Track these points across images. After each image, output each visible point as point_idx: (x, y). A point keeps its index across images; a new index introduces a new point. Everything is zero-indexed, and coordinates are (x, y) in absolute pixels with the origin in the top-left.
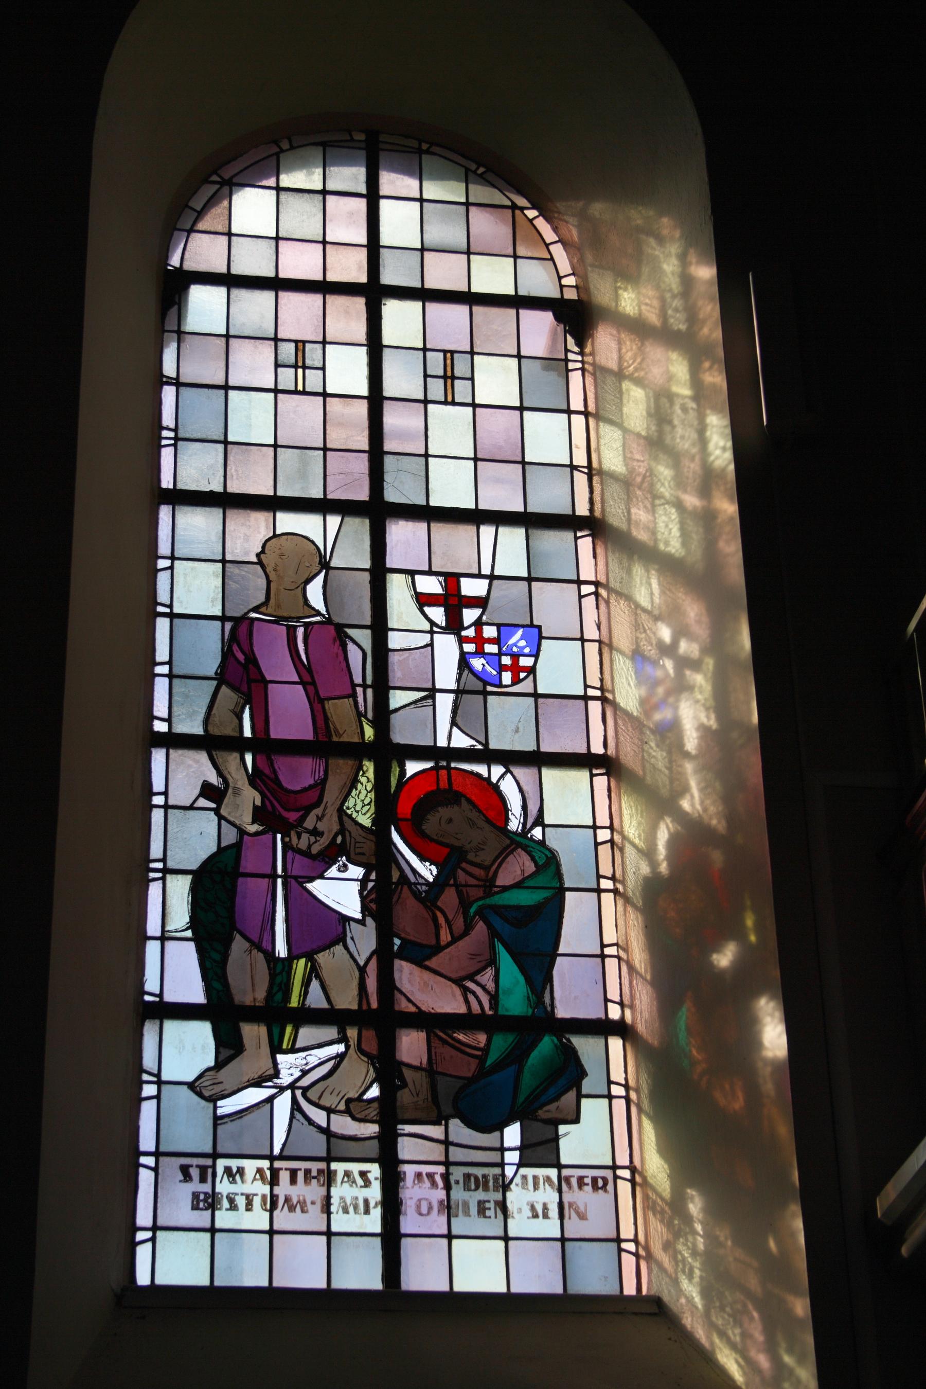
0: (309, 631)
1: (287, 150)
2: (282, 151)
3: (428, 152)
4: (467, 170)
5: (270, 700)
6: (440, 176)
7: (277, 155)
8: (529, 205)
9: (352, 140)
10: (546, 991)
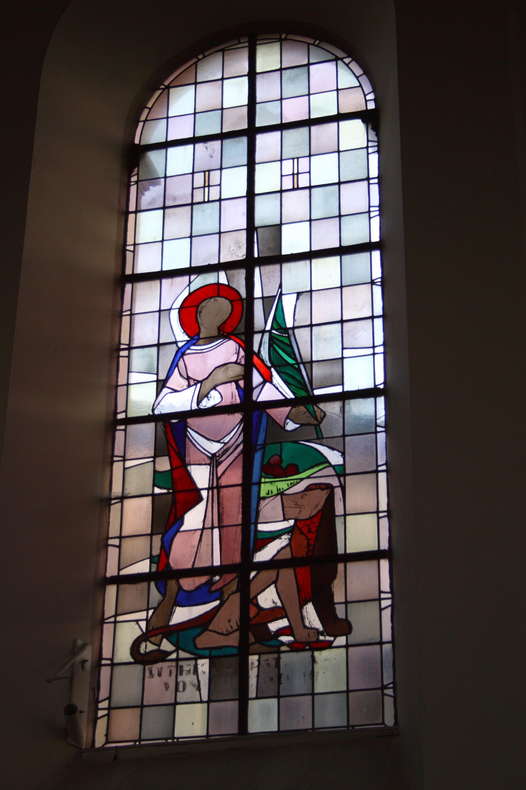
3: (286, 39)
4: (309, 44)
7: (196, 63)
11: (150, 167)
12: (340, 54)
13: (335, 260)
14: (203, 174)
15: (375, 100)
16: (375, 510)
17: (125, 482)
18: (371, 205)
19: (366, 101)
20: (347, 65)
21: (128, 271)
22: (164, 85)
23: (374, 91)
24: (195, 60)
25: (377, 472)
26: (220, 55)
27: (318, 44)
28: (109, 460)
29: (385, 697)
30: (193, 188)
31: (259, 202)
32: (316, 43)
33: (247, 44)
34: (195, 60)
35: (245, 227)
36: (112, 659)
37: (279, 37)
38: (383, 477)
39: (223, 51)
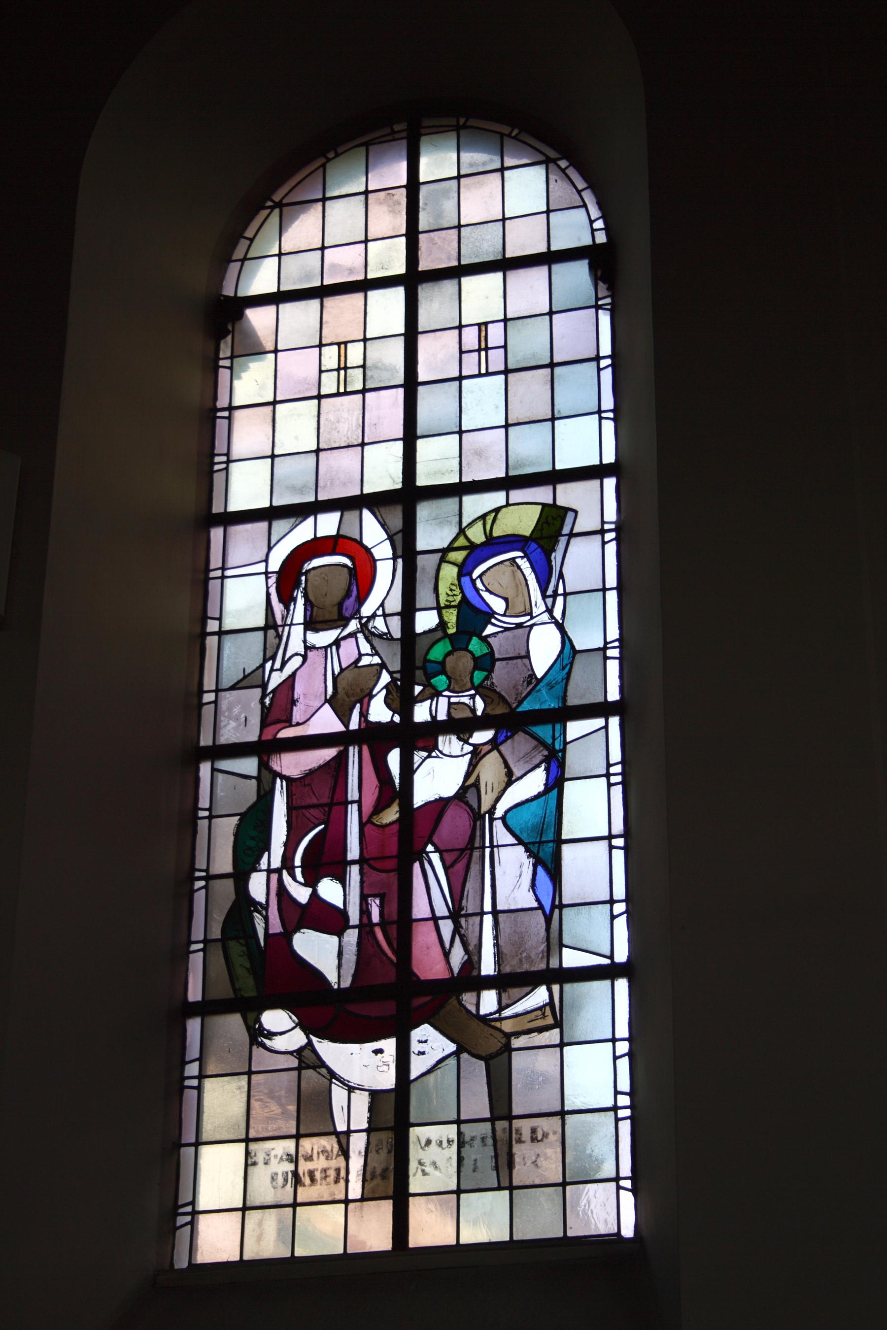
0: (266, 679)
1: (333, 158)
2: (329, 160)
3: (465, 127)
4: (502, 135)
5: (211, 1145)
6: (475, 147)
7: (324, 166)
8: (559, 156)
9: (393, 132)
10: (398, 781)
11: (251, 336)
12: (552, 154)
13: (541, 272)
14: (336, 347)
15: (607, 229)
16: (596, 409)
17: (199, 1155)
18: (605, 520)
19: (593, 231)
20: (563, 171)
21: (217, 508)
22: (273, 201)
23: (604, 217)
24: (323, 160)
25: (604, 590)
26: (363, 150)
27: (517, 135)
28: (202, 576)
29: (621, 1191)
30: (321, 372)
31: (424, 344)
32: (513, 134)
33: (404, 134)
34: (322, 160)
35: (403, 331)
36: (207, 870)
37: (455, 123)
38: (612, 598)
39: (367, 145)
